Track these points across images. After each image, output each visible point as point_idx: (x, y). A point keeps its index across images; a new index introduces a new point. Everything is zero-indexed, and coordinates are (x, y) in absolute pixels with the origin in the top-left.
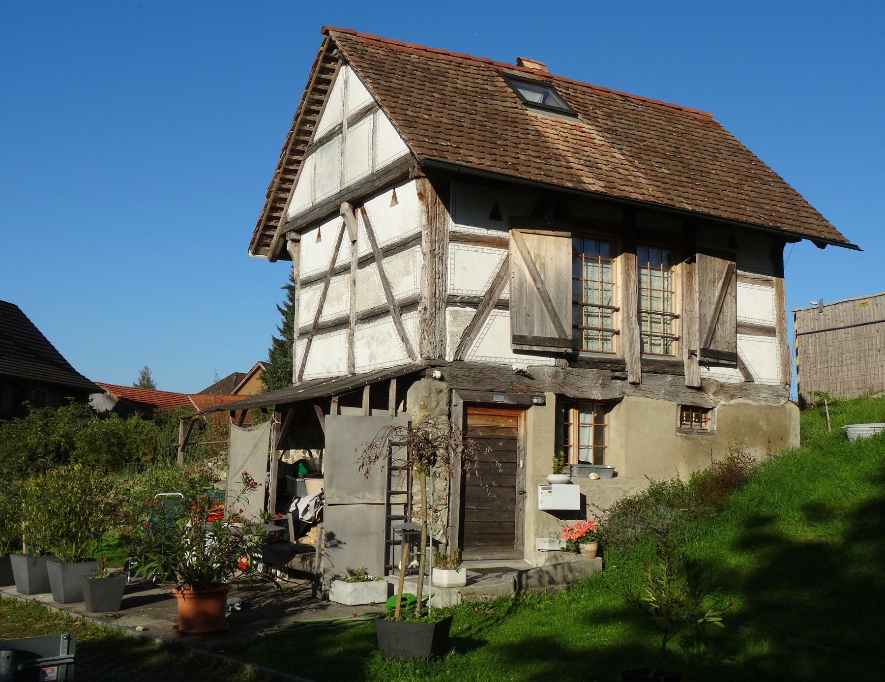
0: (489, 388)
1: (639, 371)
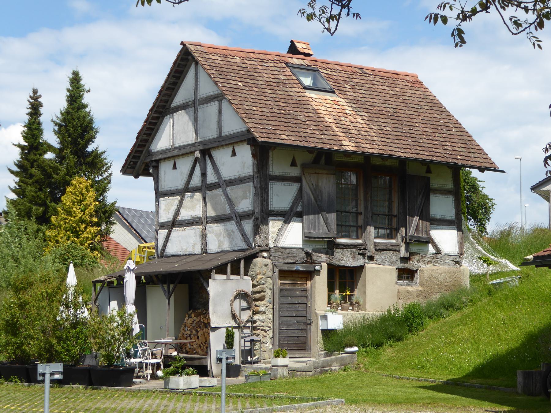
0: (292, 262)
1: (374, 249)
